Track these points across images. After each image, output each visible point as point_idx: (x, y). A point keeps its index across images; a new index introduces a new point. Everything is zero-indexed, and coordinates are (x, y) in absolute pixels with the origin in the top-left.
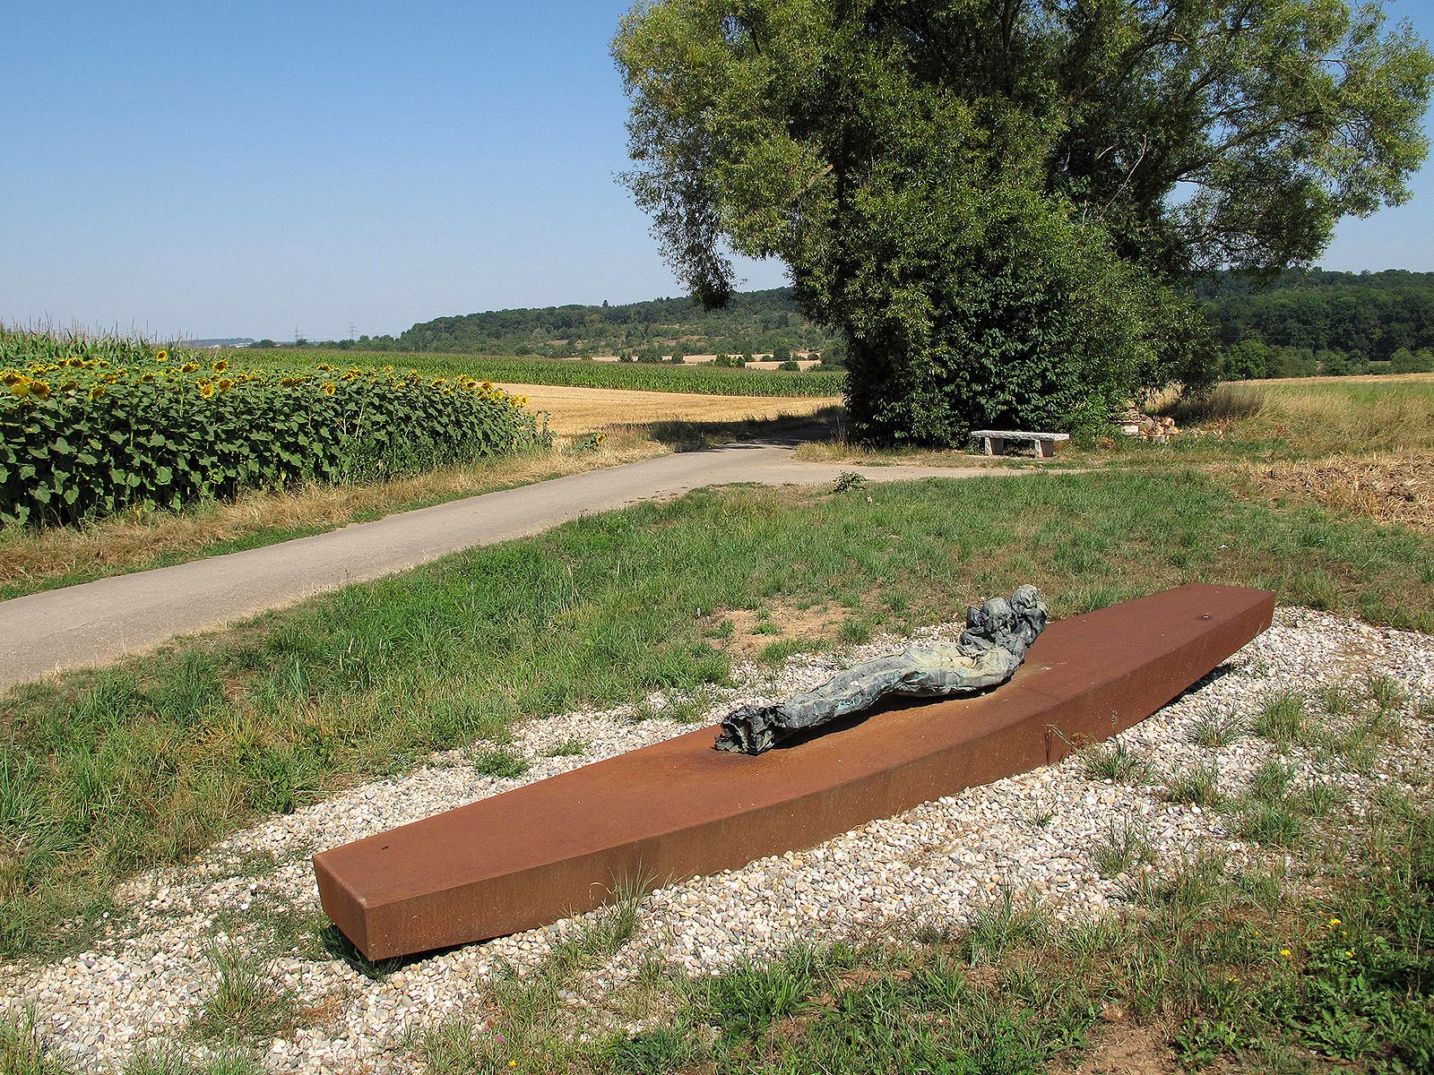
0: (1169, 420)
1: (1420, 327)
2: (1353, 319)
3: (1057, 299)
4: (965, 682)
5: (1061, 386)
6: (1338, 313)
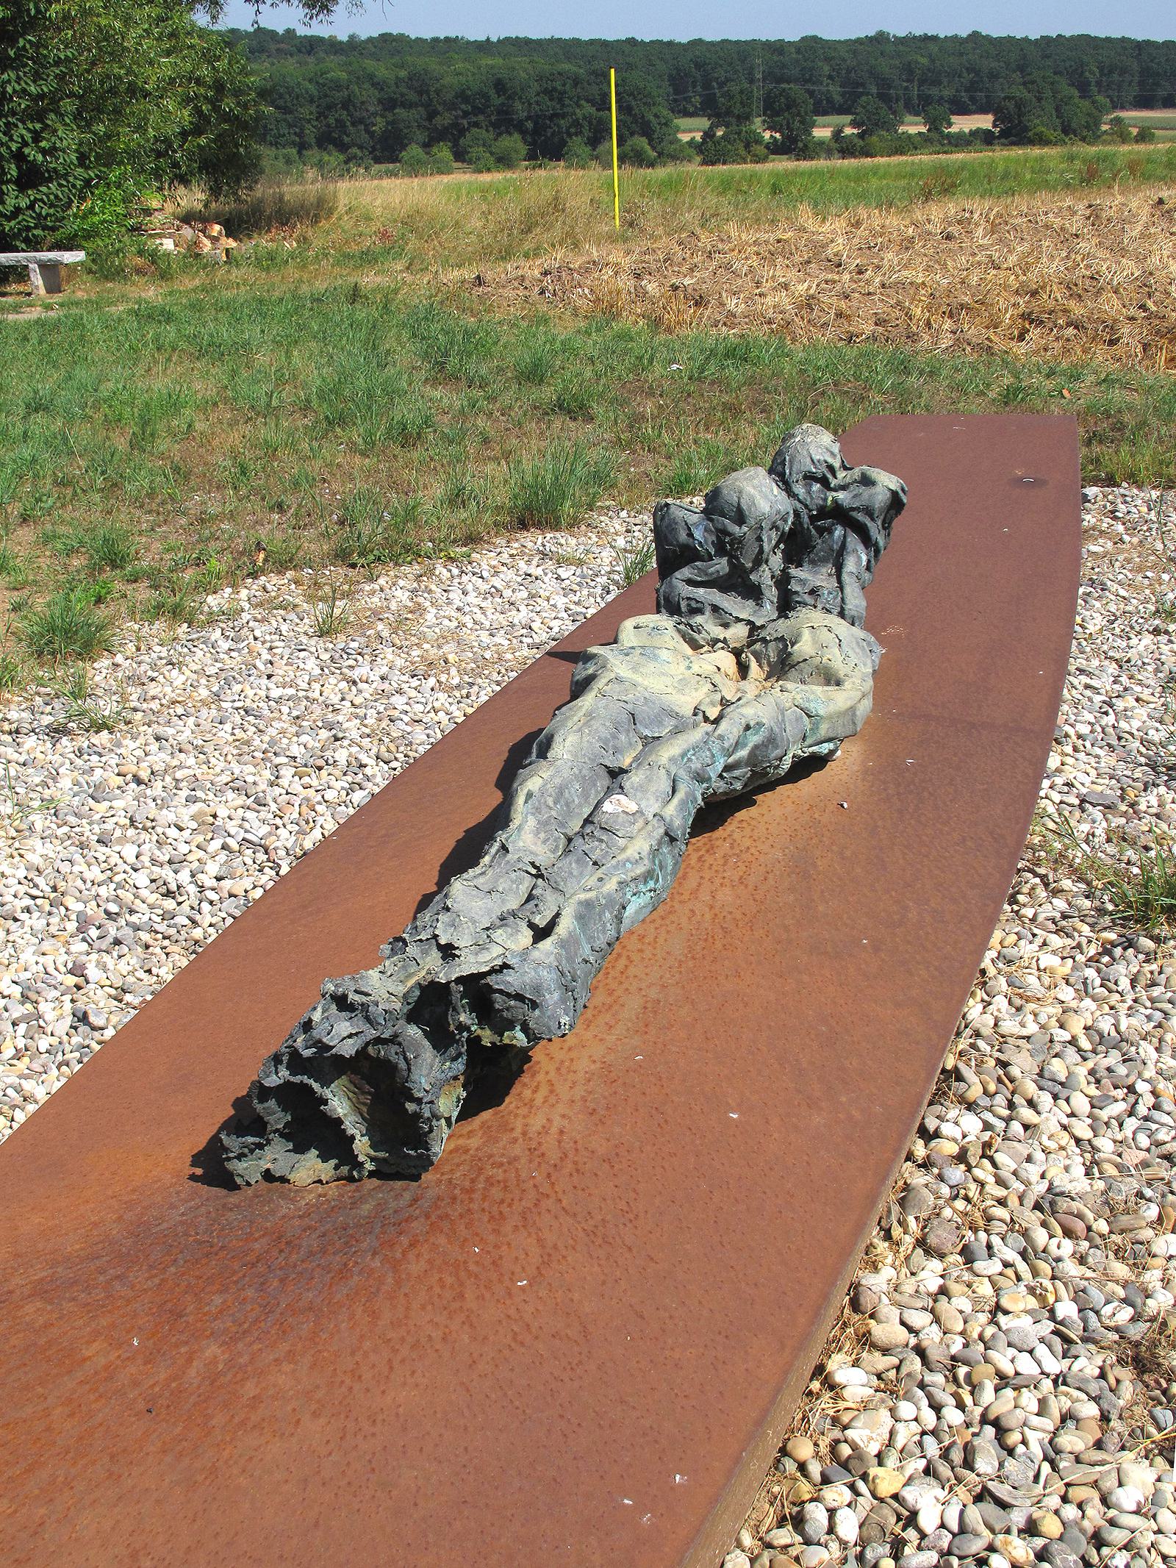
0: (217, 227)
1: (432, 115)
2: (347, 103)
3: (29, 15)
4: (824, 730)
5: (48, 171)
6: (326, 96)
